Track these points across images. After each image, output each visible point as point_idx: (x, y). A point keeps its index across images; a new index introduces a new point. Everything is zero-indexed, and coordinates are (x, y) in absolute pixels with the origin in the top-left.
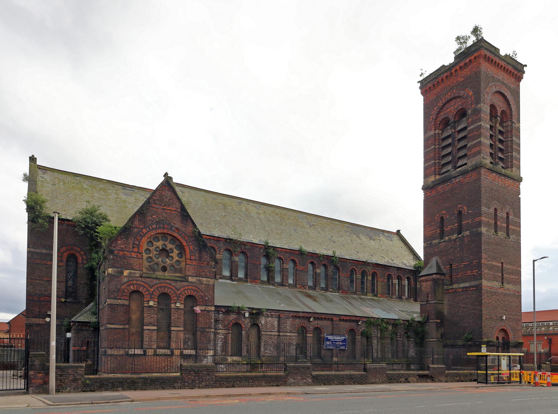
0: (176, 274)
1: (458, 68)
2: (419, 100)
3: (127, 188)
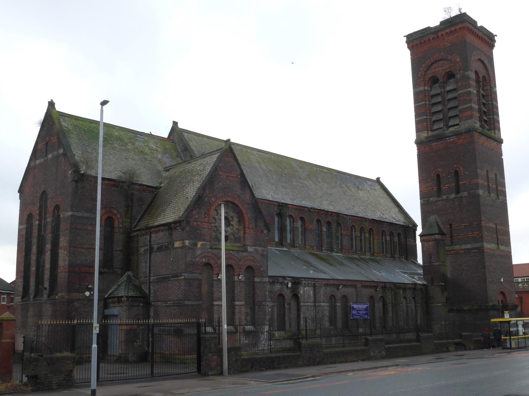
0: (236, 243)
1: (444, 33)
2: (406, 54)
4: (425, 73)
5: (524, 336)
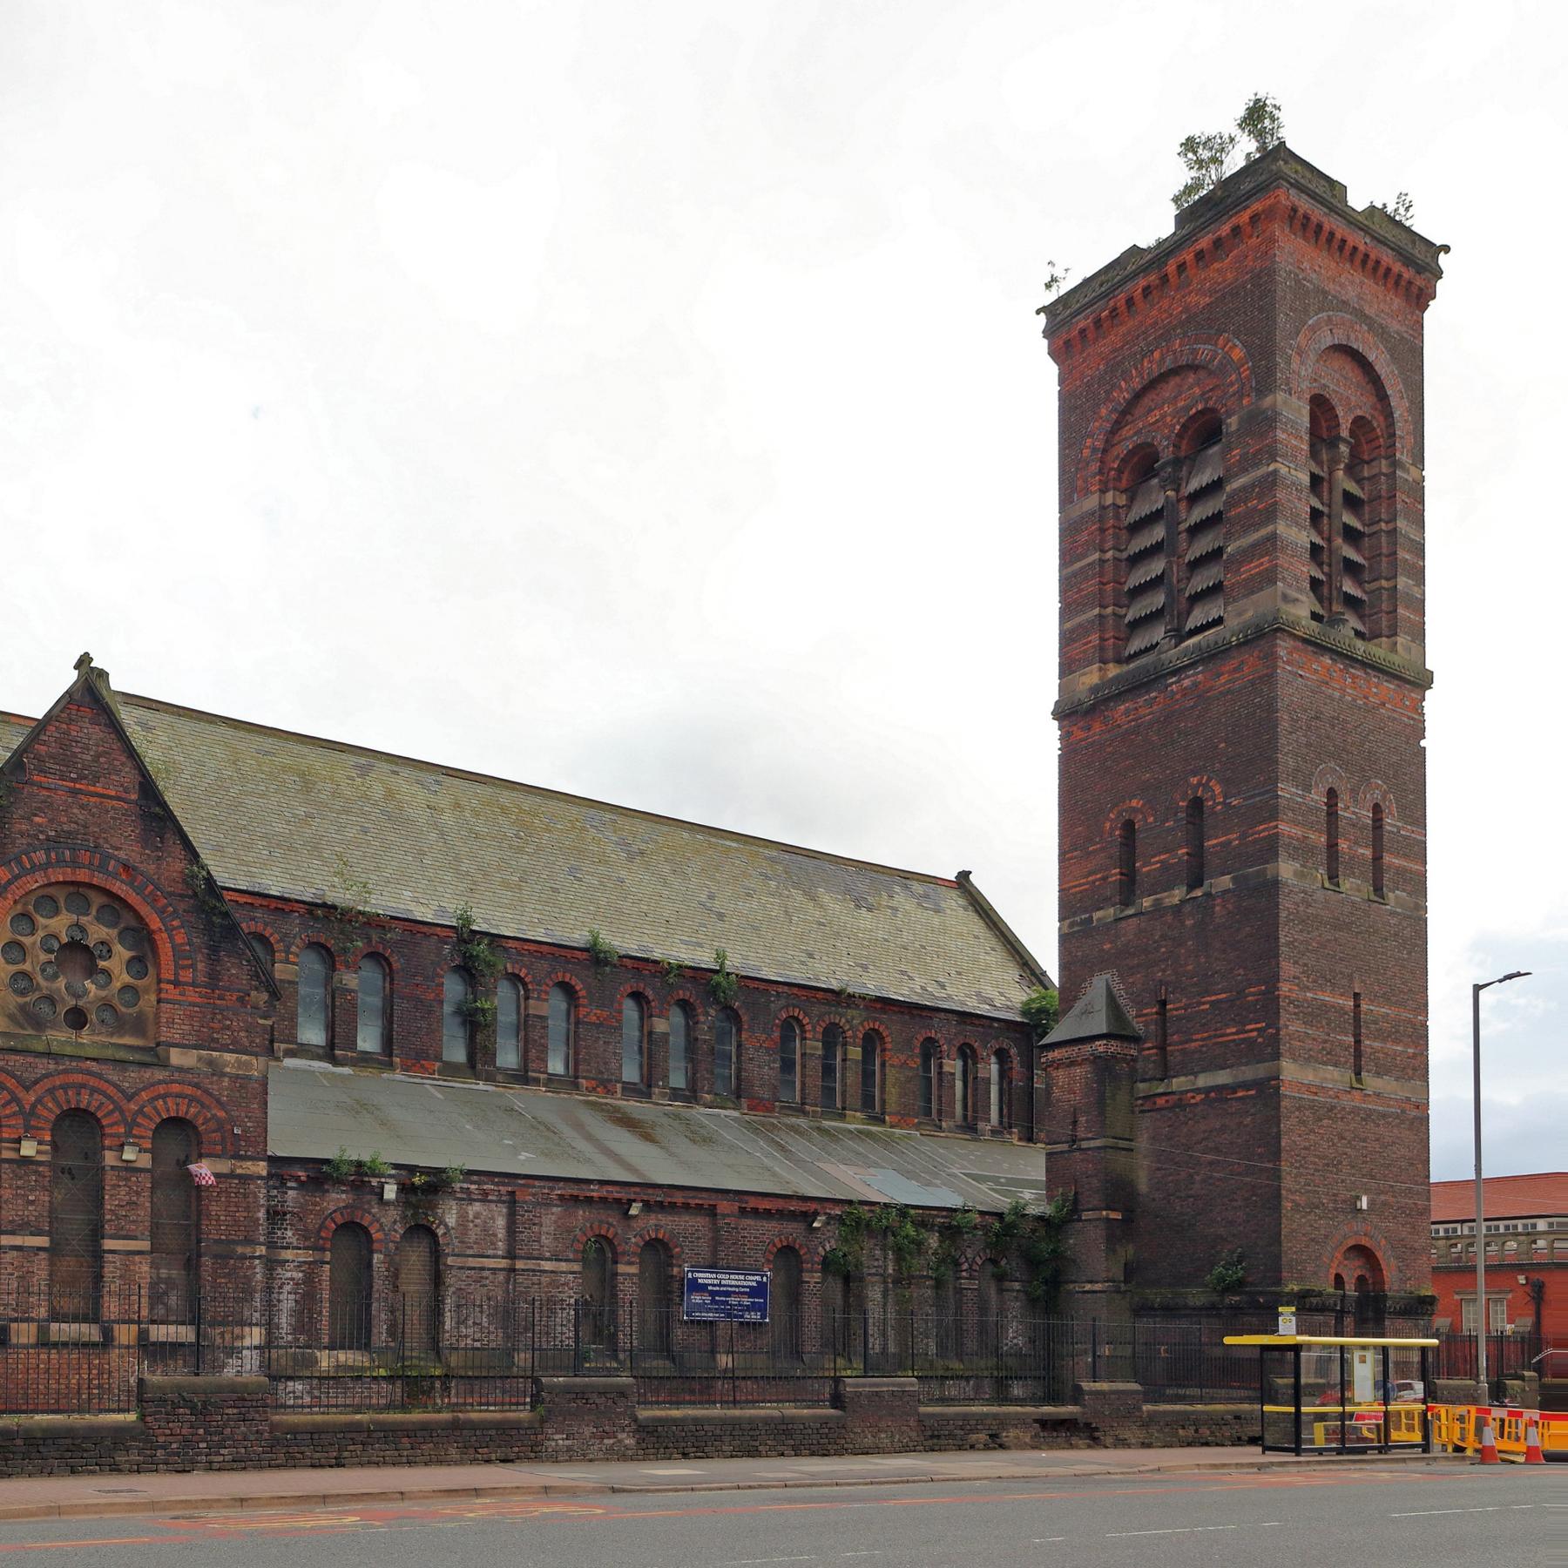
0: (121, 1036)
1: (1188, 256)
4: (1107, 441)
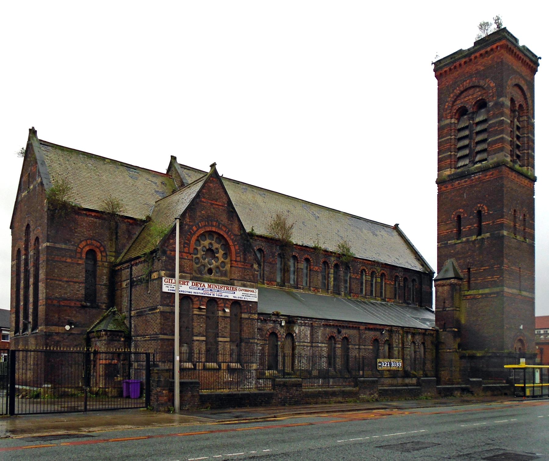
1: (478, 54)
3: (131, 169)
5: (541, 385)
